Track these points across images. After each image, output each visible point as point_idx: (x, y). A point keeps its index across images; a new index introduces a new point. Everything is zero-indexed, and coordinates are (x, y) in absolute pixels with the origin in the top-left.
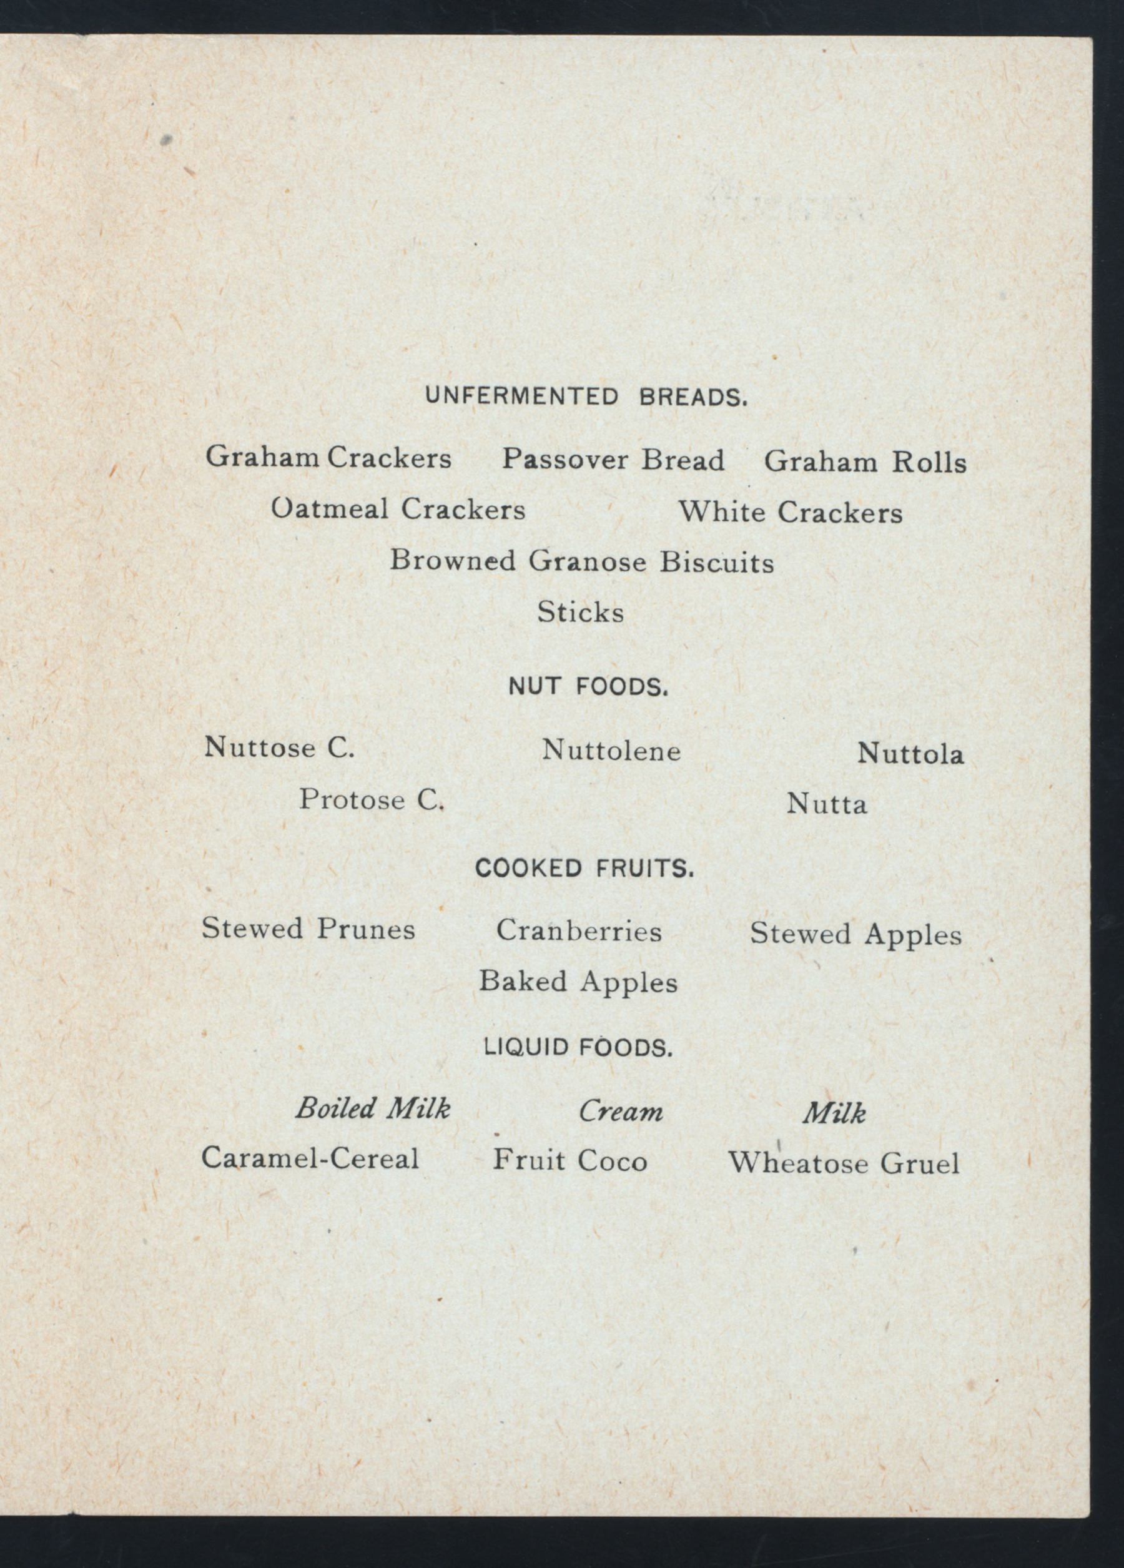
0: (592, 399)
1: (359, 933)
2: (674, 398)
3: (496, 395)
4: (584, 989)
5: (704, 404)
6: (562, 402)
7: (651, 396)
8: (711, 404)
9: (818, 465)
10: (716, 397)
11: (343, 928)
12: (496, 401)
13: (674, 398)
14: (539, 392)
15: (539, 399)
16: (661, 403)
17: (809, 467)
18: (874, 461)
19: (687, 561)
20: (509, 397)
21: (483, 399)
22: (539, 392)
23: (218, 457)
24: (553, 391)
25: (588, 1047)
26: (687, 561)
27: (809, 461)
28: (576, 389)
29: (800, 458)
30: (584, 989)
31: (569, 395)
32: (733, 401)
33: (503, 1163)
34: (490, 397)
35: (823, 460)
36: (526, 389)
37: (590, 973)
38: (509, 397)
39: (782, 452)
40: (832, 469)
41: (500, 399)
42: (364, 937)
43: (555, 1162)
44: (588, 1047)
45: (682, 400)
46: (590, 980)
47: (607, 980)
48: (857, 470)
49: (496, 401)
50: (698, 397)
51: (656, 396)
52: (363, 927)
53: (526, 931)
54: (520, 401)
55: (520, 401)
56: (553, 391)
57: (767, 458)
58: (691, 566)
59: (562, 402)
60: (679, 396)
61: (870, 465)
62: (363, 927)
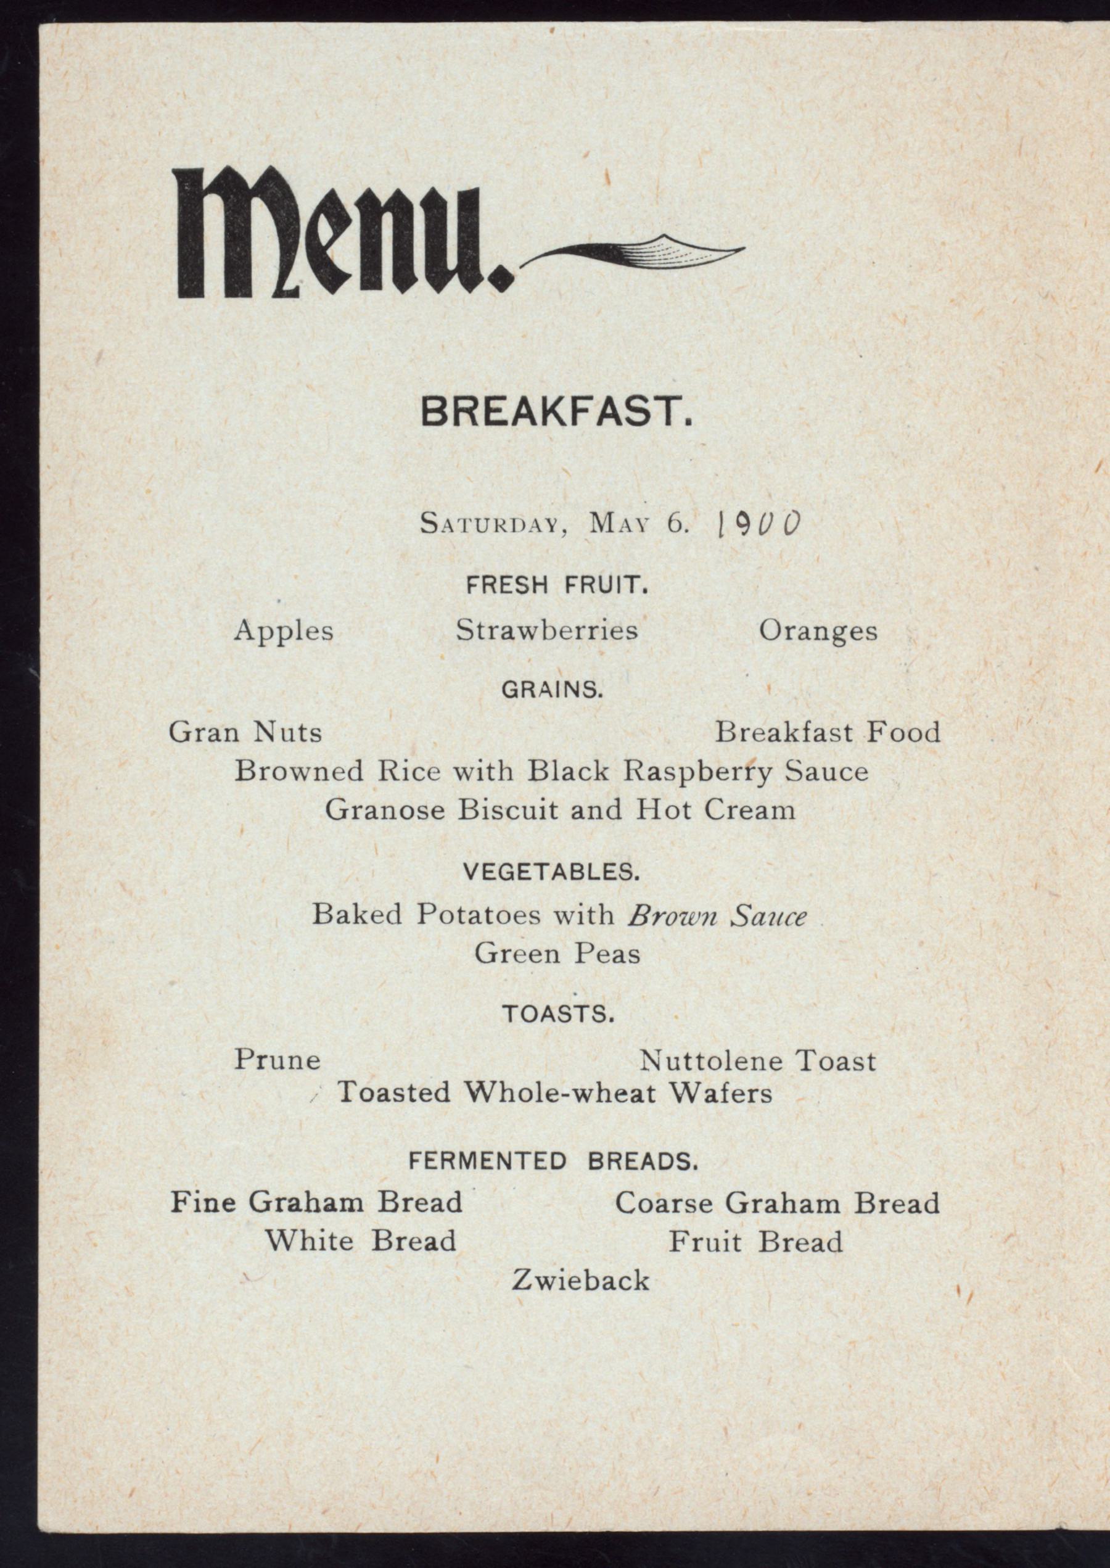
0: (540, 1164)
1: (277, 1064)
2: (623, 1162)
3: (443, 1160)
4: (237, 638)
5: (653, 1168)
6: (509, 1166)
7: (599, 1160)
8: (661, 1168)
9: (779, 1207)
10: (666, 1161)
11: (261, 1058)
12: (443, 1167)
13: (623, 1162)
14: (486, 1156)
15: (486, 1164)
16: (610, 1168)
17: (771, 1209)
18: (837, 1202)
19: (485, 808)
20: (456, 1162)
21: (430, 1164)
22: (523, 868)
23: (180, 734)
24: (500, 1155)
25: (586, 410)
26: (485, 808)
27: (771, 1203)
28: (523, 1154)
29: (761, 1200)
30: (237, 638)
31: (516, 1160)
32: (683, 1165)
33: (679, 1245)
34: (437, 1162)
35: (785, 1202)
36: (473, 1154)
37: (244, 622)
38: (456, 1162)
39: (743, 1193)
40: (793, 1211)
41: (447, 1164)
42: (282, 1067)
43: (548, 811)
44: (586, 410)
45: (631, 1164)
46: (244, 629)
47: (261, 628)
48: (819, 1211)
49: (443, 1167)
50: (648, 1161)
51: (605, 1160)
52: (281, 1058)
53: (495, 630)
54: (468, 1166)
55: (468, 1166)
56: (500, 1155)
57: (172, 726)
58: (490, 813)
59: (509, 1166)
60: (628, 1160)
61: (833, 1207)
62: (281, 1058)
